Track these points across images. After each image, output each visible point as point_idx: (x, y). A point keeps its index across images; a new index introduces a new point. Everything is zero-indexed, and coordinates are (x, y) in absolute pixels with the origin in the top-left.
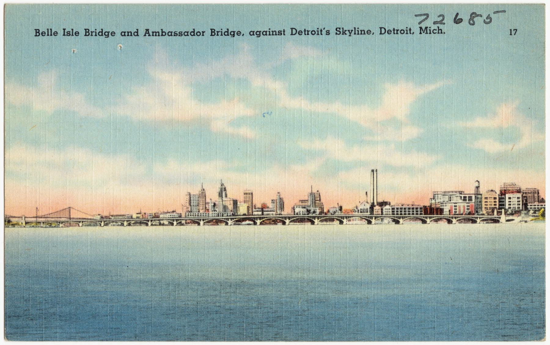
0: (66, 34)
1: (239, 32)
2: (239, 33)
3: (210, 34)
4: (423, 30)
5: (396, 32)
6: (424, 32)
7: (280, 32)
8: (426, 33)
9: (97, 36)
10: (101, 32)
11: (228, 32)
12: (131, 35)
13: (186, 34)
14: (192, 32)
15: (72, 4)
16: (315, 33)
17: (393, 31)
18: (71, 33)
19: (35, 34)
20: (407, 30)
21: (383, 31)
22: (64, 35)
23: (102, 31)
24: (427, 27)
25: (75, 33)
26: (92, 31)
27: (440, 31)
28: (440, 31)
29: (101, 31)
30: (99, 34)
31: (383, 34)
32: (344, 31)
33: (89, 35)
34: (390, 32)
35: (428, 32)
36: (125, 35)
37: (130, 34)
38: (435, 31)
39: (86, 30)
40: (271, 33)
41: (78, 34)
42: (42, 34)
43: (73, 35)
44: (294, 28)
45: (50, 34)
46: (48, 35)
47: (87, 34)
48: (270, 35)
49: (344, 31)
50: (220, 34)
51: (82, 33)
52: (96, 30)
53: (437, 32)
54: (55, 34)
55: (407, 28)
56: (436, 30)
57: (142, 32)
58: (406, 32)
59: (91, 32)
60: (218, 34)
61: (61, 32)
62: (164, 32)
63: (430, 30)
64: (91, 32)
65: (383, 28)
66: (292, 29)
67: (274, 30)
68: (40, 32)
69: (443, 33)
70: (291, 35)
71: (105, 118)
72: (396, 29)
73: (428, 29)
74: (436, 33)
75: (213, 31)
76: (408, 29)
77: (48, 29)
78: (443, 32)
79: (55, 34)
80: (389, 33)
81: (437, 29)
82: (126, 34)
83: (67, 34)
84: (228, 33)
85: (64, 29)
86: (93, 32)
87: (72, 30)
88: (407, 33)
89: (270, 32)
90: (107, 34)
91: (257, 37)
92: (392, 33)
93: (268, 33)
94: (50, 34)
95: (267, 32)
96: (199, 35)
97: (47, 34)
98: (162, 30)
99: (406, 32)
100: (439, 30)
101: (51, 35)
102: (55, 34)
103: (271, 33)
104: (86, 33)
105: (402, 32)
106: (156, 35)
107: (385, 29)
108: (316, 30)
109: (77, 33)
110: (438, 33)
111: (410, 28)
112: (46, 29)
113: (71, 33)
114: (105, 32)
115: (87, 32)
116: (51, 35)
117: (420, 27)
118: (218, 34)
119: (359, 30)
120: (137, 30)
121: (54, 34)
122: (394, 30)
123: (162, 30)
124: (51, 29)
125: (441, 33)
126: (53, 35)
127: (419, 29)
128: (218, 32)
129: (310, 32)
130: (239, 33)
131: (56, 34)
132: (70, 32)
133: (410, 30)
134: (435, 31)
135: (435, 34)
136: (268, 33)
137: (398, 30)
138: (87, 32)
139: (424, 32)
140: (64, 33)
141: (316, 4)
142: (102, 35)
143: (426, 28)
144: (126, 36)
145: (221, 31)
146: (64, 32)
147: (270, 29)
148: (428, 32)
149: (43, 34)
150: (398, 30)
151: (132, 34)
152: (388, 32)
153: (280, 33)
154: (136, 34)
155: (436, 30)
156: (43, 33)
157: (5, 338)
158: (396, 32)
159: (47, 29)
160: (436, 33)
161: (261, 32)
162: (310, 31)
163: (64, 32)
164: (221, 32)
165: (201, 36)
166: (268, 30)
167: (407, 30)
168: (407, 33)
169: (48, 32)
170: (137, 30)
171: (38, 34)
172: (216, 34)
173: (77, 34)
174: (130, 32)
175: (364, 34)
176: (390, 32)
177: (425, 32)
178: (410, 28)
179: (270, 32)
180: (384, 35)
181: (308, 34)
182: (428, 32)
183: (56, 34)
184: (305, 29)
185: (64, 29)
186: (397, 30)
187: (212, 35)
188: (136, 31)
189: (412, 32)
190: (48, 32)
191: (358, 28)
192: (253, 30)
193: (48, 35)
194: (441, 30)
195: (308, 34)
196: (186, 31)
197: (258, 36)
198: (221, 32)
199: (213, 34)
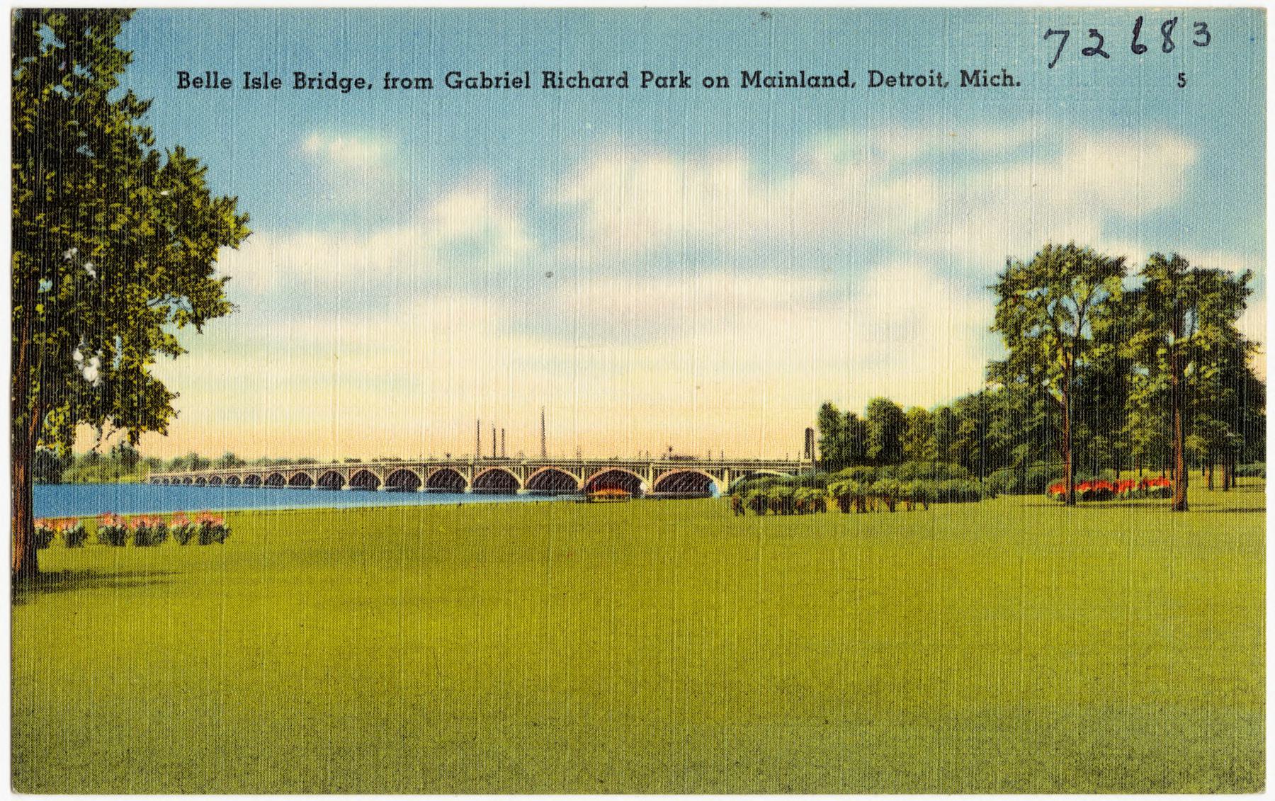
0: (250, 84)
1: (890, 79)
2: (360, 83)
3: (178, 84)
4: (749, 79)
5: (905, 81)
6: (751, 84)
7: (257, 81)
8: (975, 85)
9: (218, 87)
10: (623, 79)
11: (334, 80)
12: (832, 85)
13: (813, 82)
14: (842, 77)
15: (351, 10)
16: (925, 81)
17: (898, 81)
18: (263, 82)
19: (177, 83)
20: (932, 77)
21: (750, 79)
22: (247, 87)
23: (335, 76)
24: (979, 71)
25: (222, 83)
26: (312, 77)
27: (1008, 81)
28: (1008, 81)
29: (332, 76)
30: (809, 84)
31: (875, 86)
32: (684, 80)
33: (303, 87)
34: (892, 81)
35: (980, 83)
36: (602, 85)
37: (829, 82)
38: (996, 81)
39: (296, 74)
40: (785, 82)
41: (200, 85)
42: (194, 82)
43: (267, 87)
44: (879, 72)
45: (212, 83)
46: (208, 86)
47: (301, 84)
48: (781, 86)
49: (684, 80)
50: (316, 84)
51: (289, 80)
52: (507, 74)
53: (1001, 81)
54: (360, 83)
55: (932, 72)
56: (998, 77)
57: (860, 77)
58: (929, 81)
59: (310, 79)
60: (497, 83)
61: (238, 82)
62: (487, 79)
63: (560, 79)
64: (310, 79)
65: (647, 72)
66: (872, 73)
67: (721, 76)
68: (191, 79)
69: (1016, 84)
70: (179, 87)
71: (1199, 257)
72: (905, 74)
73: (981, 75)
74: (998, 84)
75: (299, 76)
76: (935, 75)
77: (208, 73)
78: (1015, 81)
79: (197, 84)
80: (275, 85)
81: (1001, 74)
82: (821, 82)
83: (253, 83)
84: (335, 83)
85: (247, 74)
86: (501, 79)
87: (802, 73)
88: (932, 84)
89: (781, 78)
90: (345, 83)
91: (343, 91)
92: (897, 83)
93: (777, 82)
94: (212, 83)
95: (779, 84)
96: (409, 87)
97: (524, 84)
98: (483, 74)
99: (929, 81)
100: (581, 79)
101: (216, 86)
102: (197, 84)
103: (785, 82)
104: (484, 82)
105: (921, 81)
106: (424, 87)
107: (882, 75)
108: (927, 75)
109: (361, 82)
110: (1005, 84)
111: (939, 74)
112: (262, 72)
113: (263, 82)
114: (343, 80)
115: (300, 80)
116: (216, 86)
117: (742, 72)
118: (310, 84)
119: (783, 76)
120: (846, 72)
121: (513, 84)
122: (902, 76)
123: (483, 74)
124: (216, 73)
125: (1011, 84)
126: (325, 87)
127: (960, 75)
128: (311, 80)
129: (615, 80)
130: (360, 83)
131: (360, 85)
132: (260, 79)
133: (939, 77)
134: (572, 82)
135: (996, 87)
136: (777, 82)
137: (397, 79)
138: (300, 80)
139: (751, 84)
140: (247, 83)
141: (32, 9)
142: (335, 87)
143: (758, 74)
144: (819, 86)
145: (318, 77)
146: (247, 79)
147: (507, 74)
148: (981, 81)
149: (197, 83)
150: (397, 79)
151: (835, 83)
152: (888, 81)
153: (517, 83)
154: (843, 82)
155: (998, 77)
156: (890, 79)
157: (12, 788)
158: (905, 81)
159: (801, 72)
160: (998, 84)
161: (352, 81)
162: (913, 77)
163: (247, 79)
164: (320, 80)
165: (306, 88)
166: (504, 76)
167: (932, 77)
168: (932, 83)
169: (209, 77)
170: (846, 72)
171: (185, 83)
172: (308, 85)
173: (276, 83)
174: (829, 77)
175: (725, 86)
176: (892, 81)
177: (755, 83)
178: (939, 74)
179: (781, 78)
180: (877, 88)
181: (909, 84)
182: (981, 81)
183: (227, 83)
184: (902, 74)
185: (247, 74)
186: (909, 78)
187: (297, 87)
188: (844, 75)
189: (942, 82)
190: (209, 77)
191: (561, 73)
192: (348, 77)
193: (208, 86)
194: (1011, 77)
195: (909, 84)
196: (662, 76)
197: (344, 90)
198: (507, 80)
199: (301, 84)
